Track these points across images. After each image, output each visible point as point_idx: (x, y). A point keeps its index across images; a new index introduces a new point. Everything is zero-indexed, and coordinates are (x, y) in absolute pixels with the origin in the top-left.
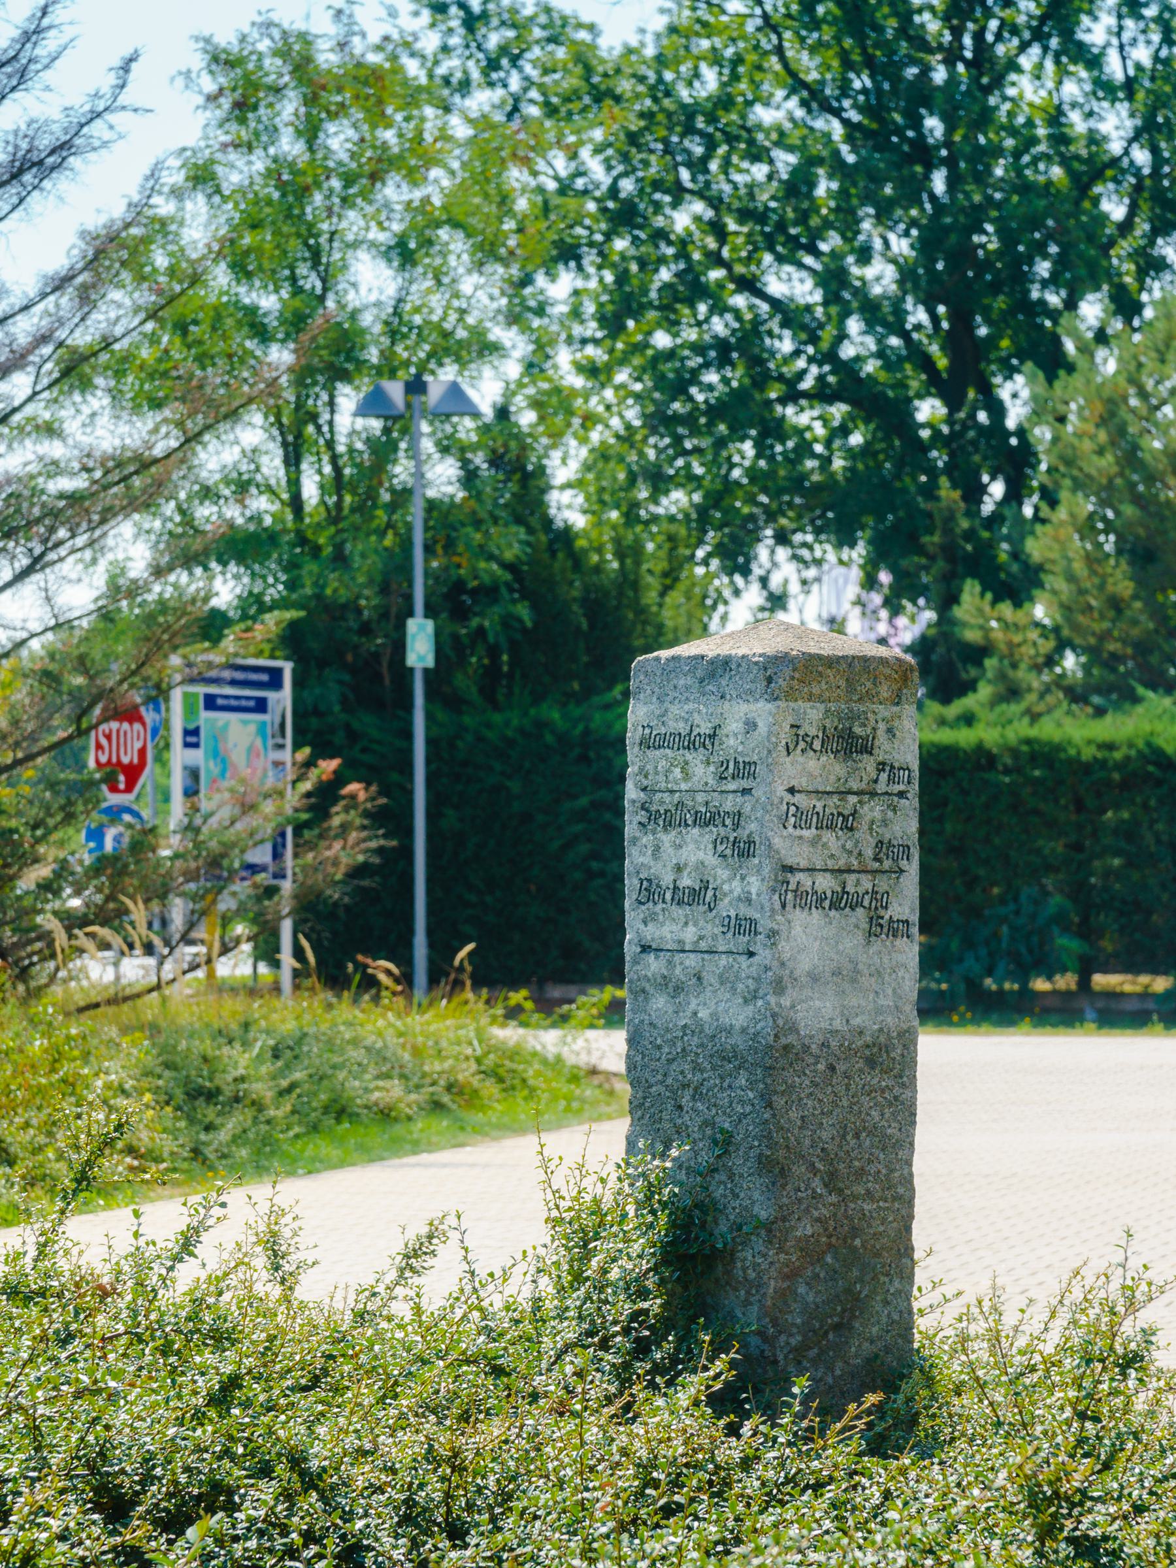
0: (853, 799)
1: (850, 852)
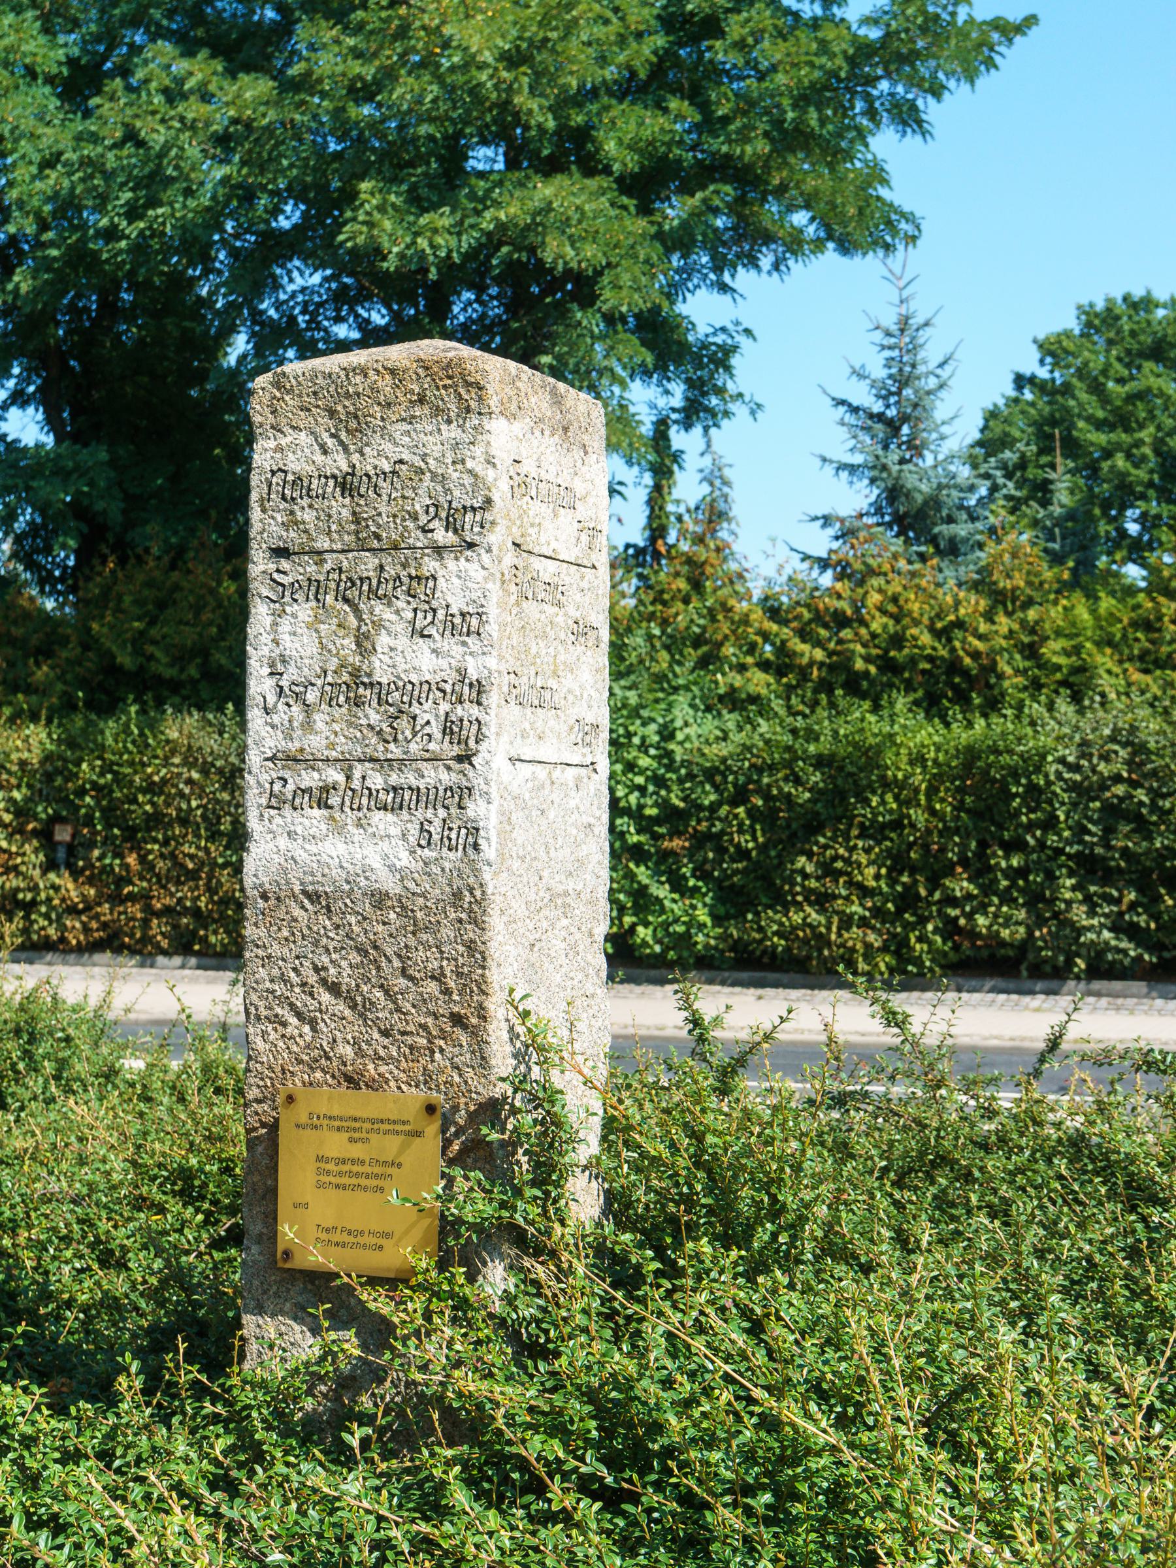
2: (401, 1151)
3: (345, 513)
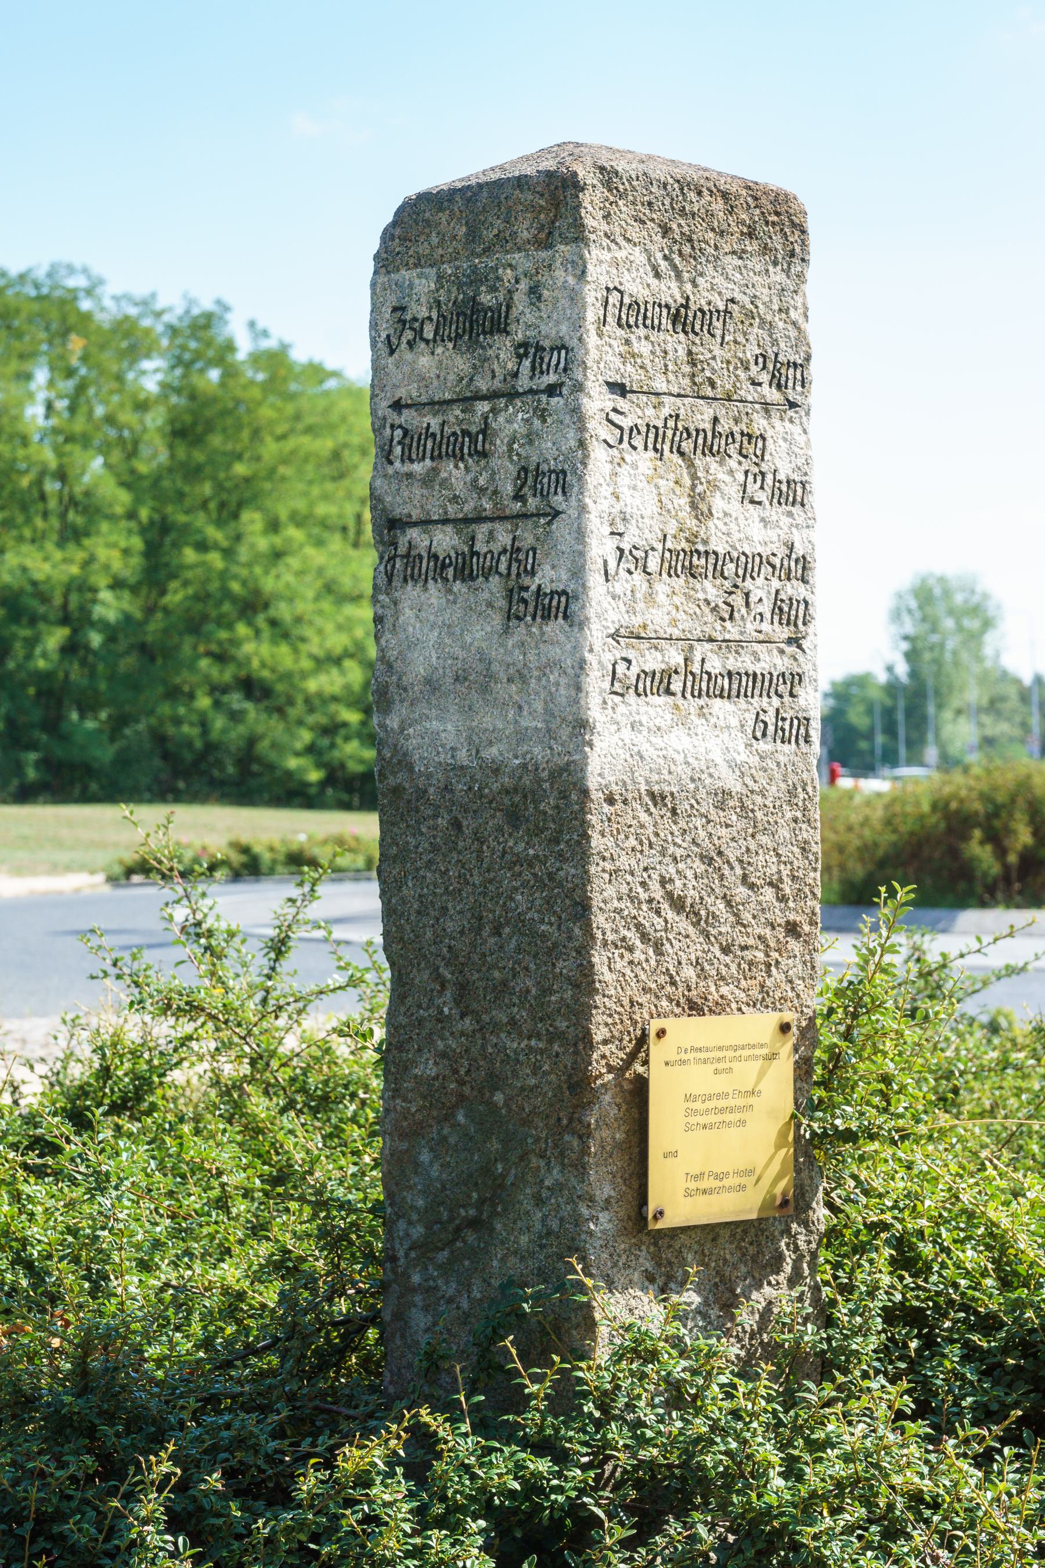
0: (483, 407)
1: (482, 491)
2: (761, 1074)
3: (682, 353)
